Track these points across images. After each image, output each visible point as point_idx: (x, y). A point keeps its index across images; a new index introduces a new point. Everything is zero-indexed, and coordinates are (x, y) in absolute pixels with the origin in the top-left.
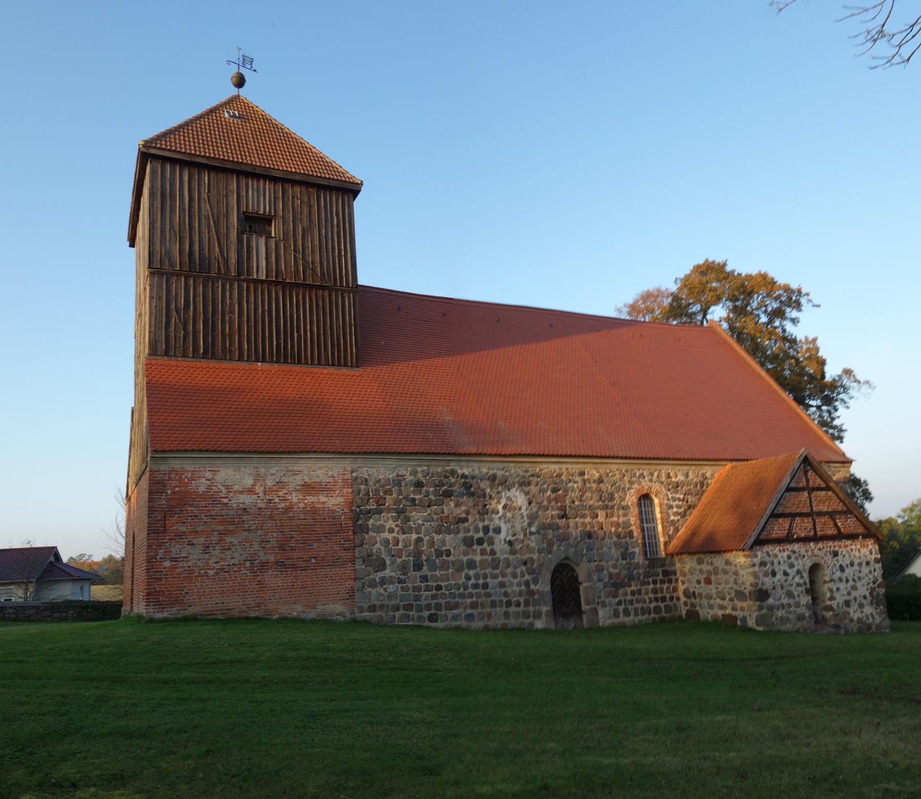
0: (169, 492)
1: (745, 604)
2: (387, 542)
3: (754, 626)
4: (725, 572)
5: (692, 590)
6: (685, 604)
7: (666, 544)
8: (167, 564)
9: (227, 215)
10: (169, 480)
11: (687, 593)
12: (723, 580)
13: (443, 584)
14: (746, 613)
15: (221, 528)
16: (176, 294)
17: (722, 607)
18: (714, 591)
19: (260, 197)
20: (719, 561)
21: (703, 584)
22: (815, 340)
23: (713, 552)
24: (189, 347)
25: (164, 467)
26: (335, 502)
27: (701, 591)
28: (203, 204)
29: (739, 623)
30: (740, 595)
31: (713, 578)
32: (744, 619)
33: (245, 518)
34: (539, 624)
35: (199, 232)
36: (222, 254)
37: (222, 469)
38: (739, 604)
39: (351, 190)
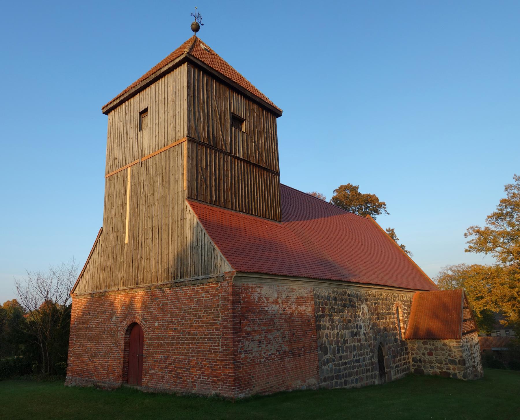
0: (242, 301)
1: (456, 367)
2: (327, 335)
3: (462, 378)
4: (443, 350)
5: (418, 359)
6: (414, 365)
7: (405, 333)
8: (243, 356)
9: (225, 112)
10: (242, 293)
11: (414, 360)
12: (441, 354)
13: (347, 361)
14: (456, 371)
15: (265, 328)
16: (201, 158)
17: (439, 368)
18: (435, 359)
19: (239, 106)
20: (439, 344)
21: (426, 355)
22: (393, 230)
23: (435, 339)
24: (207, 195)
25: (239, 284)
26: (308, 309)
27: (425, 359)
28: (213, 101)
29: (451, 376)
30: (453, 362)
31: (434, 352)
32: (455, 374)
33: (275, 321)
34: (377, 382)
35: (212, 120)
36: (223, 138)
37: (264, 286)
38: (451, 367)
39: (276, 113)
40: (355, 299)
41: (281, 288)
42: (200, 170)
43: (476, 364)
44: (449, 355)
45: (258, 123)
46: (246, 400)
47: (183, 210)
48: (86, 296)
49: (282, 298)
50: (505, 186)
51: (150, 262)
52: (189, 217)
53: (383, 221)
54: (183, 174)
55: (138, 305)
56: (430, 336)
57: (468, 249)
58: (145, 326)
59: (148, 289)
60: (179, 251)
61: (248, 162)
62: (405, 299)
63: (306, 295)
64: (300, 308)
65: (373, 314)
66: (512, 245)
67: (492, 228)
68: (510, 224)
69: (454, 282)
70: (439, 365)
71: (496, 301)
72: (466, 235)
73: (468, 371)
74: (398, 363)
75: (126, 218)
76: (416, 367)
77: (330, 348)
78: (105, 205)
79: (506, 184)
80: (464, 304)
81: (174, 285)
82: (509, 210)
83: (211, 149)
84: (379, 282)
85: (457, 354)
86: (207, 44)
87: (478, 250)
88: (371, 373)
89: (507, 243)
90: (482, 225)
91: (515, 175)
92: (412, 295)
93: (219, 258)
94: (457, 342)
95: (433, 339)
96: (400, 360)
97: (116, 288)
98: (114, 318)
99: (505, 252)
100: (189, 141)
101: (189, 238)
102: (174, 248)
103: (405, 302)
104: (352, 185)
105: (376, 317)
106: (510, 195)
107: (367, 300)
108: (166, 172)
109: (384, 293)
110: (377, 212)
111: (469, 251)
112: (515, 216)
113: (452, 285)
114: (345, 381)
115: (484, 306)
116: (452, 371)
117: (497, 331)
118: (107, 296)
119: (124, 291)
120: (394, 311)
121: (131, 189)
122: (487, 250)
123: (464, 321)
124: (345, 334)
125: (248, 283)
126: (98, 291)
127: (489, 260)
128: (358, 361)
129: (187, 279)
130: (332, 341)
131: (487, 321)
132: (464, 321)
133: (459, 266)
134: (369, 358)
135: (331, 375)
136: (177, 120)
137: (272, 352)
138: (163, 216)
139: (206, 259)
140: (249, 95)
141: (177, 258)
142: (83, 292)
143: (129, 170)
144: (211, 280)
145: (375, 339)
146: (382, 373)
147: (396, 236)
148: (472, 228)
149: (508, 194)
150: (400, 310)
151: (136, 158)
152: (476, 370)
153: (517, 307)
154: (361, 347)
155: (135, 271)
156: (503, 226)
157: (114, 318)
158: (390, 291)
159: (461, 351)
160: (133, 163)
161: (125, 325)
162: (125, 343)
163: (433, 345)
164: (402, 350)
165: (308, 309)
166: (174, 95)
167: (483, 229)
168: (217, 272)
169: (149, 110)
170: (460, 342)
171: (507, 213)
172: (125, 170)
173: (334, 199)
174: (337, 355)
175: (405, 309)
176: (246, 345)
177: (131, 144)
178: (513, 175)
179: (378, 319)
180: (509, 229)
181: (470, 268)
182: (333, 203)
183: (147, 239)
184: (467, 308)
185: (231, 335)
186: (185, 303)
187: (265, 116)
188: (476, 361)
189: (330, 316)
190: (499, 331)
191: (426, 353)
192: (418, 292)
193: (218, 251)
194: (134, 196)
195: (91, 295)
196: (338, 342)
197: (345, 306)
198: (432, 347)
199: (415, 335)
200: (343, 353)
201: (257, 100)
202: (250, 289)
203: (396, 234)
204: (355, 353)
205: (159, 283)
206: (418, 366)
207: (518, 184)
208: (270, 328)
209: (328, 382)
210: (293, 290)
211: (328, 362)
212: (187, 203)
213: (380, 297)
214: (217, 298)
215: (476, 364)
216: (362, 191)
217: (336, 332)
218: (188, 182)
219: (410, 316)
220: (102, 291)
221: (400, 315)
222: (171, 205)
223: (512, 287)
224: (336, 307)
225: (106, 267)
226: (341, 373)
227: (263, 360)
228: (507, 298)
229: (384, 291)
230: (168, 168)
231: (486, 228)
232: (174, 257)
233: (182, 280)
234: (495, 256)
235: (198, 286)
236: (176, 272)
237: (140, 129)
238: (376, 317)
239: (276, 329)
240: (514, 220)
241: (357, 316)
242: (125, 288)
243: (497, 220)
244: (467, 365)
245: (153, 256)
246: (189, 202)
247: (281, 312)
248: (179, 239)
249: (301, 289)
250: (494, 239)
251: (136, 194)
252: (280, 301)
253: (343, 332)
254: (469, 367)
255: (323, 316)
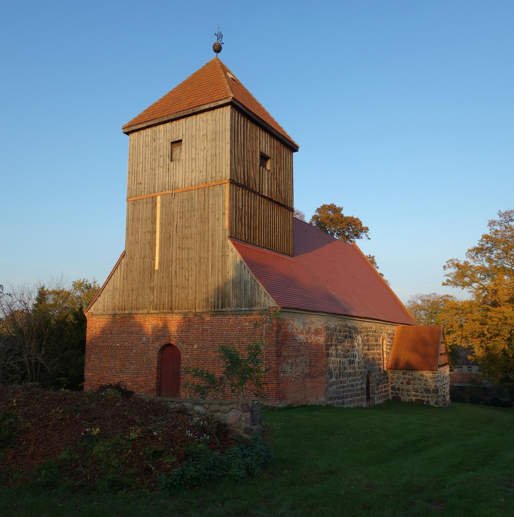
1: (430, 395)
3: (434, 405)
4: (420, 379)
5: (397, 387)
6: (392, 393)
8: (282, 375)
9: (256, 152)
11: (393, 388)
13: (345, 385)
14: (430, 399)
17: (415, 396)
18: (412, 388)
21: (405, 384)
22: (373, 257)
23: (414, 370)
26: (321, 339)
27: (403, 387)
29: (425, 403)
31: (412, 382)
32: (428, 401)
34: (364, 406)
39: (293, 148)
40: (353, 331)
41: (305, 320)
42: (238, 210)
43: (445, 393)
44: (425, 385)
45: (279, 161)
46: (285, 409)
47: (224, 247)
48: (106, 316)
49: (305, 330)
50: (489, 221)
51: (186, 291)
52: (231, 255)
53: (364, 245)
54: (224, 214)
55: (173, 328)
56: (409, 368)
57: (446, 282)
58: (182, 347)
59: (185, 315)
60: (220, 284)
61: (271, 200)
62: (389, 332)
63: (320, 327)
64: (317, 338)
65: (365, 345)
66: (487, 282)
67: (471, 262)
68: (489, 260)
69: (422, 313)
70: (415, 393)
71: (466, 336)
72: (445, 267)
73: (440, 399)
74: (380, 390)
75: (155, 246)
76: (394, 395)
77: (335, 373)
78: (127, 229)
79: (490, 220)
80: (442, 340)
81: (215, 313)
82: (489, 245)
83: (246, 189)
84: (371, 316)
85: (432, 385)
86: (234, 74)
87: (456, 285)
88: (360, 397)
89: (483, 279)
90: (462, 259)
91: (500, 211)
92: (395, 328)
93: (263, 294)
94: (433, 373)
95: (412, 370)
96: (382, 388)
97: (145, 311)
98: (144, 339)
99: (480, 289)
100: (231, 183)
101: (231, 273)
102: (214, 281)
103: (389, 334)
104: (335, 206)
105: (367, 347)
106: (493, 230)
107: (361, 332)
108: (204, 209)
109: (374, 326)
110: (358, 236)
111: (447, 284)
112: (495, 252)
113: (420, 315)
114: (343, 401)
115: (454, 341)
116: (426, 399)
117: (459, 367)
118: (134, 318)
119: (156, 315)
120: (380, 343)
121: (161, 218)
122: (464, 285)
123: (441, 354)
124: (345, 361)
125: (286, 316)
126: (121, 312)
127: (463, 295)
128: (352, 386)
129: (229, 309)
130: (336, 367)
131: (455, 356)
132: (441, 354)
133: (430, 296)
134: (360, 384)
135: (334, 396)
136: (218, 161)
137: (299, 373)
138: (202, 249)
139: (250, 293)
140: (275, 133)
141: (218, 290)
142: (101, 311)
143: (159, 199)
144: (256, 312)
145: (365, 367)
146: (368, 398)
147: (376, 264)
148: (452, 260)
149: (490, 230)
150: (385, 342)
151: (167, 188)
152: (445, 399)
153: (485, 344)
154: (355, 374)
155: (168, 298)
156: (482, 262)
157: (144, 339)
158: (378, 324)
159: (436, 381)
160: (164, 192)
161: (158, 345)
162: (158, 361)
163: (412, 375)
164: (384, 379)
165: (321, 339)
166: (214, 134)
167: (462, 263)
168: (261, 306)
169: (183, 142)
170: (436, 373)
171: (488, 248)
172: (154, 199)
173: (315, 218)
174: (339, 379)
175: (389, 342)
176: (283, 366)
177: (160, 172)
178: (498, 211)
179: (368, 350)
180: (487, 265)
181: (441, 298)
182: (314, 224)
183: (183, 268)
184: (443, 343)
185: (274, 358)
186: (227, 330)
187: (285, 151)
188: (446, 392)
189: (336, 346)
190: (461, 367)
191: (405, 383)
192: (401, 326)
193: (262, 288)
194: (165, 226)
195: (114, 315)
196: (340, 368)
197: (346, 337)
198: (410, 377)
199: (395, 366)
200: (343, 378)
201: (281, 137)
202: (287, 322)
203: (376, 261)
204: (350, 378)
205: (198, 311)
206: (396, 394)
207: (501, 221)
208: (298, 354)
209: (331, 401)
210: (313, 323)
211: (332, 385)
212: (229, 242)
213: (371, 330)
214: (261, 327)
215: (445, 393)
216: (346, 213)
217: (339, 359)
218: (230, 222)
219: (393, 348)
220: (126, 312)
221: (385, 347)
222: (210, 241)
223: (483, 324)
224: (340, 338)
225: (131, 292)
226: (341, 395)
227: (293, 379)
228: (477, 334)
229: (374, 324)
230: (207, 205)
231: (465, 263)
232: (215, 289)
233: (224, 310)
234: (470, 292)
235: (241, 316)
236: (216, 302)
237: (172, 161)
238: (367, 347)
239: (302, 355)
240: (493, 256)
241: (354, 347)
242: (156, 312)
243: (477, 254)
244: (439, 394)
245: (190, 285)
246: (231, 240)
247: (305, 341)
248: (220, 273)
249: (317, 322)
250: (472, 275)
251: (167, 224)
252: (304, 332)
253: (344, 360)
254: (441, 395)
255: (331, 345)
